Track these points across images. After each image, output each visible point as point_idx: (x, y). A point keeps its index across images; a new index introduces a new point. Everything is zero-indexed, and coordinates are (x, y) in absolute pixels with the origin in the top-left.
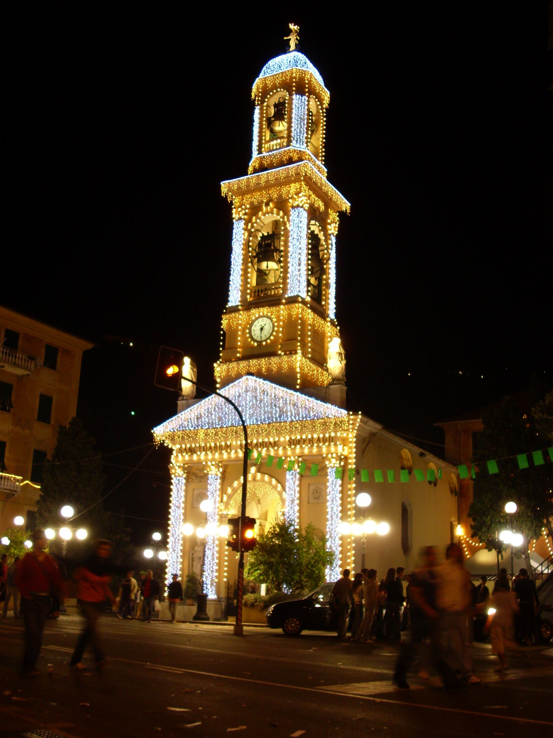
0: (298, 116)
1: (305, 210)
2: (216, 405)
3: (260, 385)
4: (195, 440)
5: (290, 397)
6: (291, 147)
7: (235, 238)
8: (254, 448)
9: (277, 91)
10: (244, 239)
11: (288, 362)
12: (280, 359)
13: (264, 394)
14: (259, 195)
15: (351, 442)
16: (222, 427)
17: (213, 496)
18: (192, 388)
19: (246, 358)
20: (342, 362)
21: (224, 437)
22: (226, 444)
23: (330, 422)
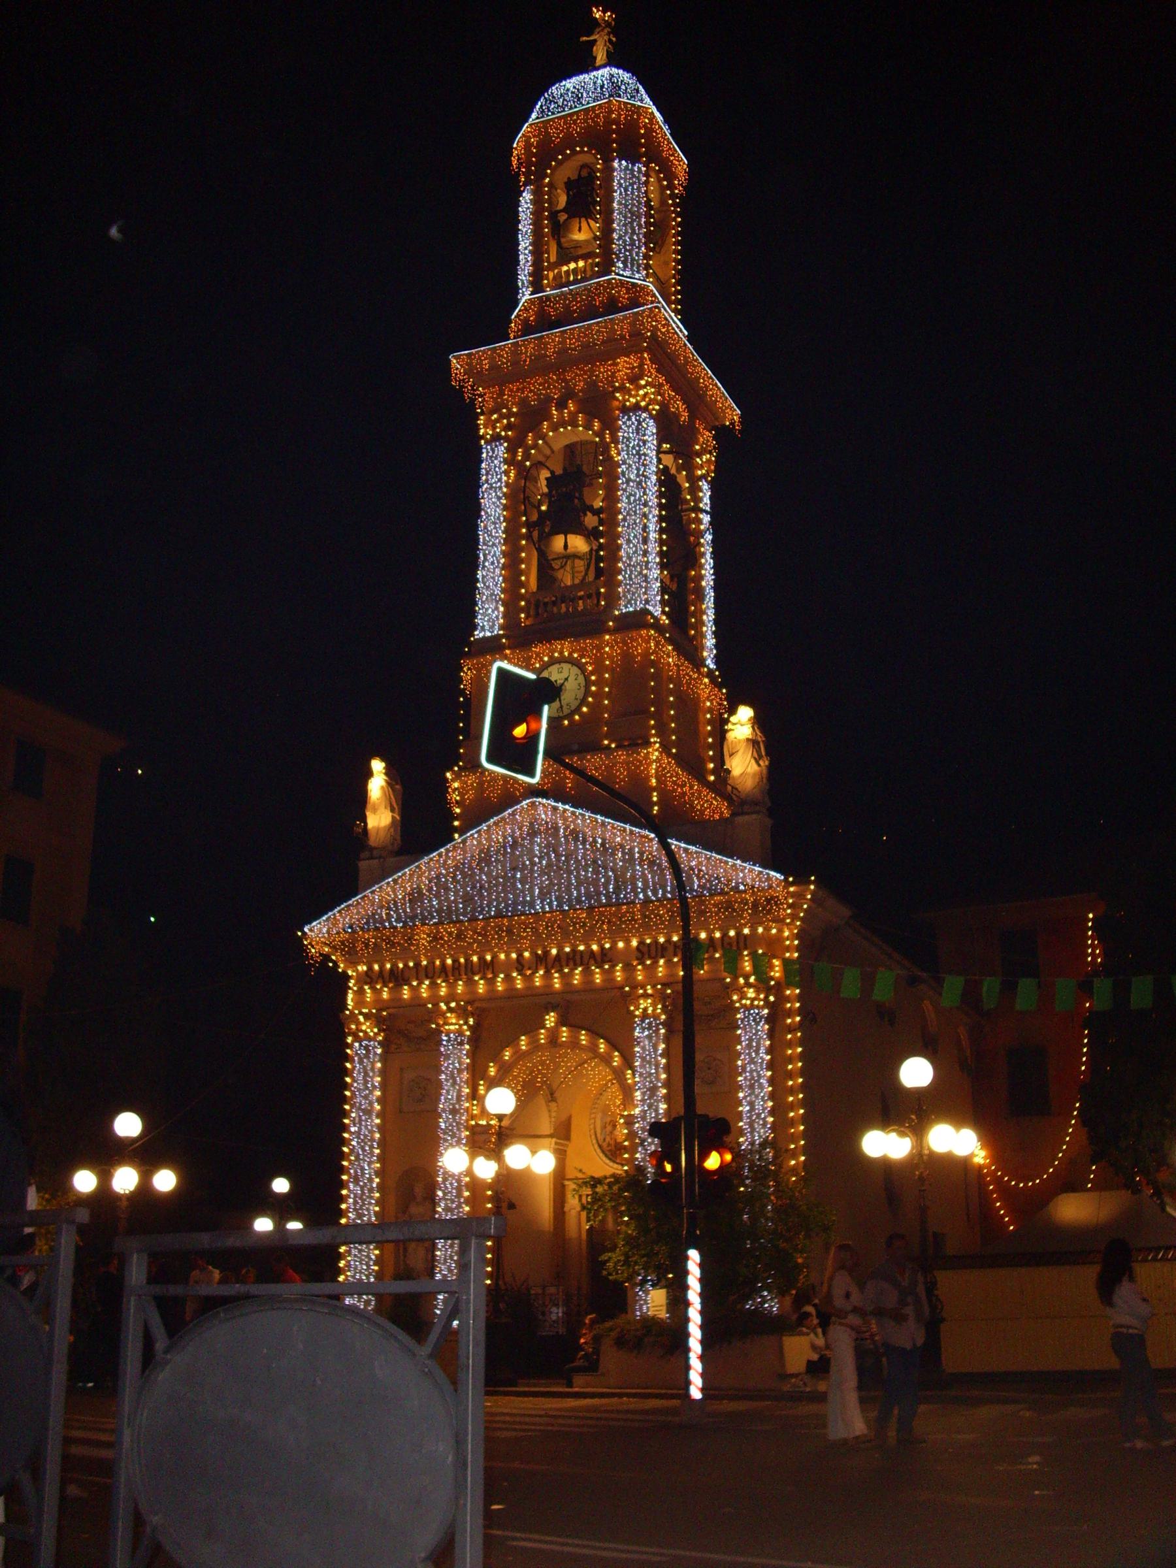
0: (626, 206)
1: (651, 417)
2: (457, 867)
3: (565, 819)
4: (406, 954)
5: (642, 843)
6: (613, 276)
7: (487, 481)
8: (553, 967)
9: (574, 152)
10: (507, 485)
11: (628, 763)
12: (607, 757)
13: (576, 839)
14: (540, 385)
15: (788, 949)
16: (473, 919)
17: (454, 1083)
18: (392, 830)
20: (761, 763)
21: (479, 942)
22: (482, 959)
23: (742, 900)
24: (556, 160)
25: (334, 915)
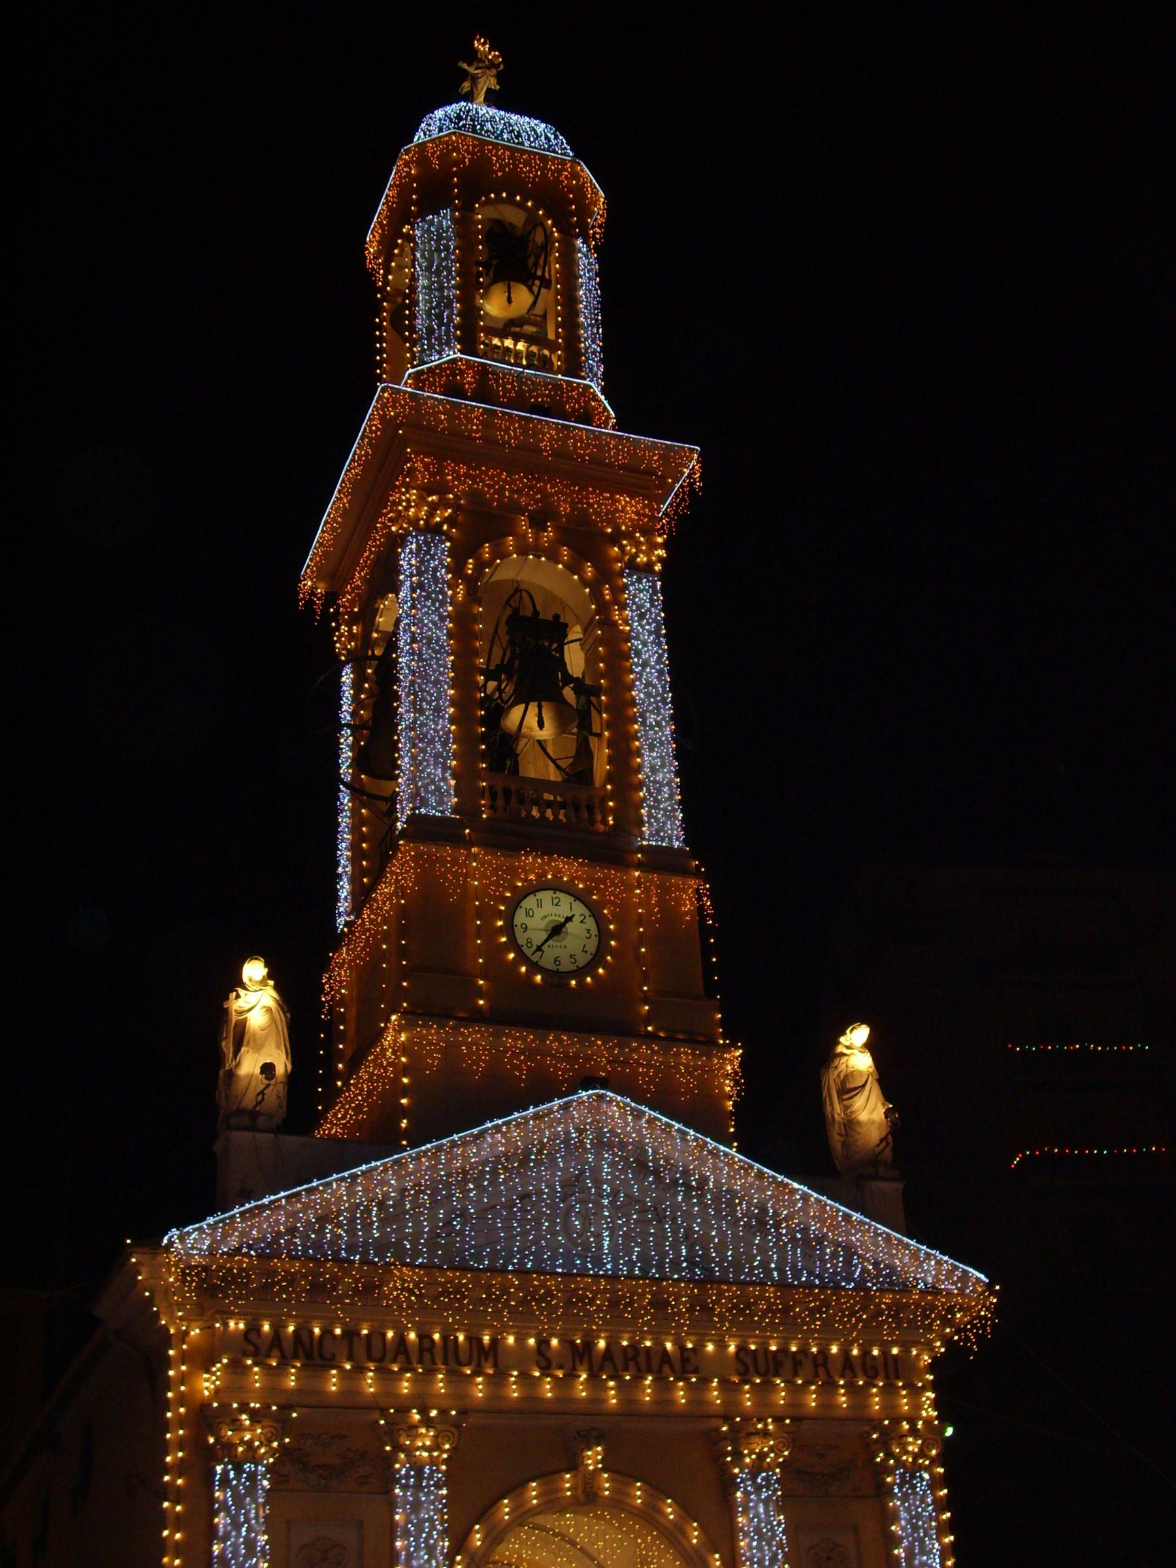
19: (496, 1018)
24: (498, 194)
25: (956, 1268)
